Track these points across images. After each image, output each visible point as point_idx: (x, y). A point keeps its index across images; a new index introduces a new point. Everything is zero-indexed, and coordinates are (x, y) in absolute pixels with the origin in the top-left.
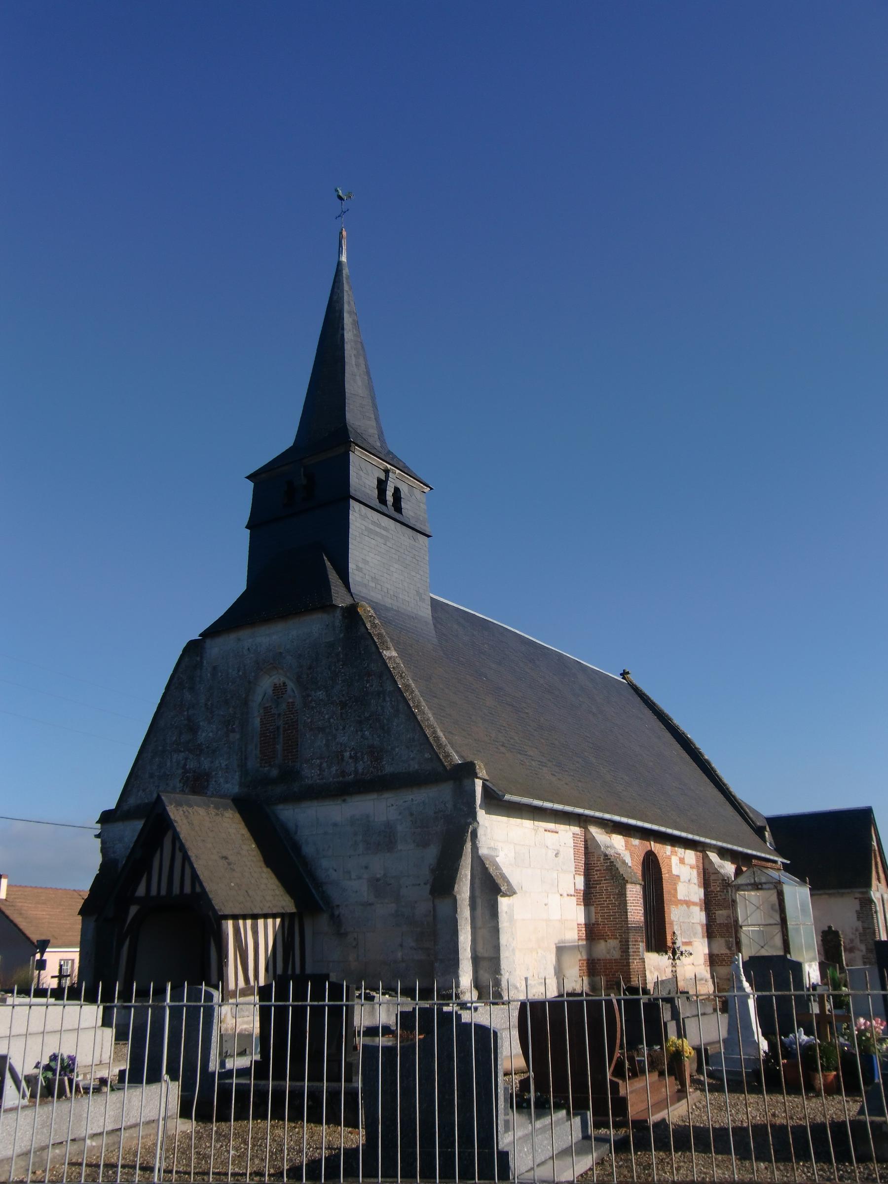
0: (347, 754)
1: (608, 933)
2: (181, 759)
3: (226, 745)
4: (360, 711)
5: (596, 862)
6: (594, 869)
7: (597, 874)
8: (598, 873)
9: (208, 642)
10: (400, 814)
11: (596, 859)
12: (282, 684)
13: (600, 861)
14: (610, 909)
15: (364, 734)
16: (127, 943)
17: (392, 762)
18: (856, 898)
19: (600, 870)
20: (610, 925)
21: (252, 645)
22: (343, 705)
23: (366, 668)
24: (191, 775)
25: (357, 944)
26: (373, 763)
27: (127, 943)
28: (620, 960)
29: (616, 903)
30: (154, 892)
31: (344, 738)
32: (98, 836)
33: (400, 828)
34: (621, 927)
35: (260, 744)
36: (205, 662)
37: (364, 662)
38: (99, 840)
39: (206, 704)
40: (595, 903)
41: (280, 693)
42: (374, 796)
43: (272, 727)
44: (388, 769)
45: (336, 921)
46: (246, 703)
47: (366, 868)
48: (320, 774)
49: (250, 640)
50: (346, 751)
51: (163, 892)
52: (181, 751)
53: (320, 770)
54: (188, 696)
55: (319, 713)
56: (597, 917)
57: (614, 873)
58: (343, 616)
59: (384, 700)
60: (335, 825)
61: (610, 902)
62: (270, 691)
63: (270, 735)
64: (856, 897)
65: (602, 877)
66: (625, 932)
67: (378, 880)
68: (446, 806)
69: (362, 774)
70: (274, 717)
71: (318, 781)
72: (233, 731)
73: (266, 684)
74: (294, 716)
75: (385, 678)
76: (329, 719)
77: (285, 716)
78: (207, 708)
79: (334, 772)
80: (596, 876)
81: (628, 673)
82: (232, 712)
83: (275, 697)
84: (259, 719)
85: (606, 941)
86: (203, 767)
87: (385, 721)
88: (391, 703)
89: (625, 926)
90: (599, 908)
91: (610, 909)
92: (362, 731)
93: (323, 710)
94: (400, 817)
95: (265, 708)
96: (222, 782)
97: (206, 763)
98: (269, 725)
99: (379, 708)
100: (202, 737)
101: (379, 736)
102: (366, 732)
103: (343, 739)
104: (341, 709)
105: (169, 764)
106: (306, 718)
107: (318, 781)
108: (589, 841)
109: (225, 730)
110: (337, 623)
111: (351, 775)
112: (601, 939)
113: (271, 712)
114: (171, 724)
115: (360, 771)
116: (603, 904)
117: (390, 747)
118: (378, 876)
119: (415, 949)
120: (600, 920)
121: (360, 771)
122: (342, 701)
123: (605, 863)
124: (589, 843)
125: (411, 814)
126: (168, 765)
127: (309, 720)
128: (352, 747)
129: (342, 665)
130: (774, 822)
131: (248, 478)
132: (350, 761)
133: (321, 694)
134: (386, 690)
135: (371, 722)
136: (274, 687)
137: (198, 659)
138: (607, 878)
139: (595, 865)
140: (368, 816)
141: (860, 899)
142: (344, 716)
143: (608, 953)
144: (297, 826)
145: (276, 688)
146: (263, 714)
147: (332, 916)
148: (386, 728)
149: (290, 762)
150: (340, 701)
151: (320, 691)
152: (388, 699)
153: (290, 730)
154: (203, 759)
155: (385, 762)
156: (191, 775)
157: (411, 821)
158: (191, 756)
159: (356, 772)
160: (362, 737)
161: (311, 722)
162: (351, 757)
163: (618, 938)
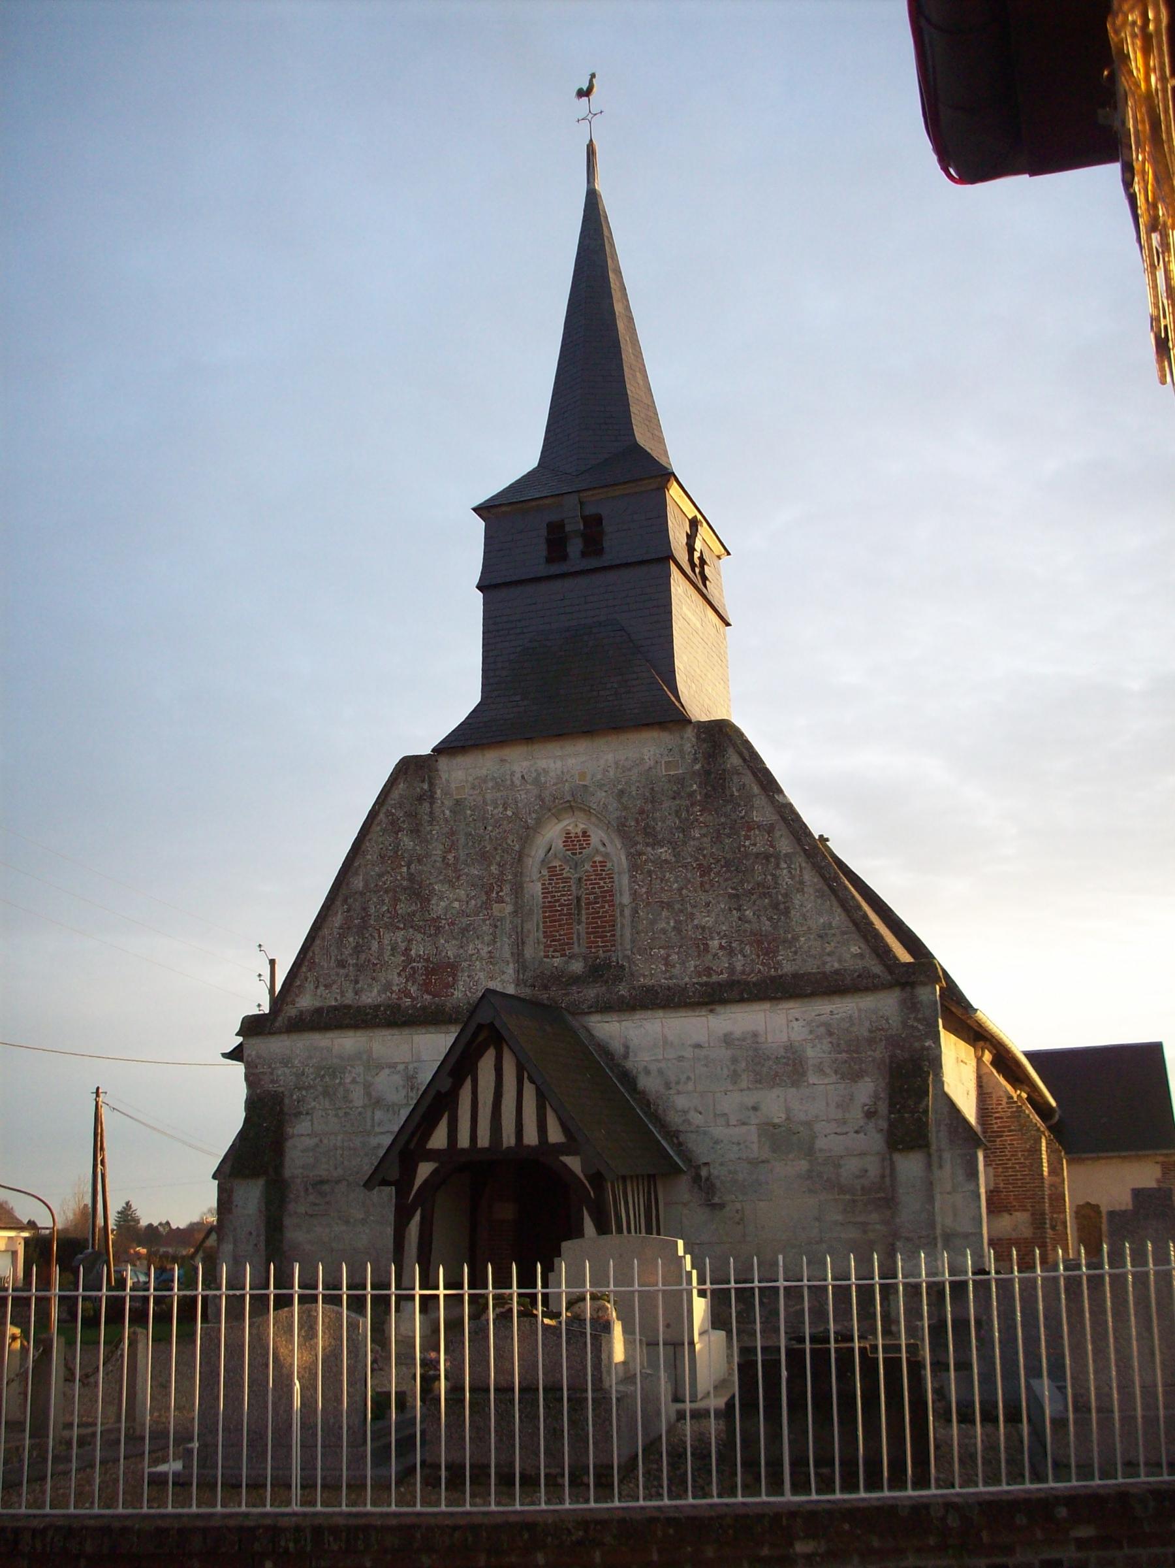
0: (714, 944)
1: (1015, 1204)
2: (399, 940)
3: (488, 922)
4: (735, 881)
5: (994, 1106)
6: (991, 1116)
7: (996, 1123)
8: (998, 1121)
9: (443, 763)
10: (811, 1032)
11: (994, 1102)
12: (581, 834)
13: (1001, 1104)
14: (1018, 1171)
15: (744, 915)
16: (417, 1218)
17: (795, 957)
18: (1157, 1163)
19: (1002, 1118)
20: (1016, 1193)
21: (529, 771)
22: (705, 871)
23: (743, 818)
24: (420, 965)
25: (742, 1219)
26: (762, 957)
27: (417, 1218)
28: (1032, 1238)
29: (1027, 1162)
30: (464, 1141)
31: (707, 919)
32: (235, 1054)
33: (810, 1053)
34: (1033, 1195)
35: (545, 922)
36: (439, 792)
37: (740, 809)
38: (239, 1068)
39: (444, 858)
40: (994, 1163)
41: (577, 847)
42: (766, 1006)
43: (565, 898)
44: (788, 968)
45: (705, 1187)
46: (520, 857)
47: (755, 1108)
48: (667, 971)
49: (525, 764)
50: (712, 939)
51: (484, 1141)
52: (398, 928)
53: (666, 965)
54: (407, 842)
55: (662, 880)
56: (997, 1181)
57: (1023, 1121)
58: (698, 737)
59: (777, 866)
60: (698, 1046)
61: (1017, 1161)
62: (559, 844)
63: (563, 910)
64: (1157, 1160)
65: (1005, 1127)
66: (1039, 1202)
67: (775, 1126)
68: (889, 1023)
69: (743, 972)
70: (570, 882)
71: (663, 981)
72: (500, 900)
73: (553, 833)
74: (605, 883)
75: (778, 834)
76: (680, 889)
77: (588, 882)
78: (447, 864)
79: (692, 969)
80: (995, 1126)
81: (827, 840)
82: (497, 872)
83: (569, 853)
84: (539, 885)
85: (1011, 1214)
86: (443, 954)
87: (780, 897)
88: (790, 872)
89: (1040, 1193)
90: (1000, 1170)
91: (1018, 1171)
92: (740, 910)
93: (668, 875)
94: (810, 1037)
95: (549, 868)
96: (481, 977)
97: (450, 950)
98: (559, 894)
99: (769, 877)
100: (438, 907)
101: (770, 919)
102: (747, 912)
103: (709, 921)
104: (701, 876)
105: (375, 945)
106: (637, 887)
107: (663, 981)
108: (984, 1077)
109: (484, 898)
110: (688, 747)
111: (722, 973)
112: (1003, 1211)
113: (562, 874)
114: (376, 885)
115: (739, 968)
116: (1006, 1164)
117: (790, 936)
118: (776, 1121)
119: (842, 1224)
120: (1002, 1185)
121: (739, 968)
122: (702, 864)
123: (1009, 1108)
124: (985, 1080)
125: (830, 1034)
126: (373, 949)
127: (644, 890)
128: (722, 934)
129: (700, 811)
130: (1038, 1058)
131: (475, 509)
132: (721, 953)
133: (664, 852)
134: (780, 852)
135: (754, 897)
136: (566, 837)
137: (426, 786)
138: (1013, 1128)
139: (993, 1111)
140: (755, 1035)
141: (1163, 1164)
142: (707, 886)
143: (1014, 1230)
144: (627, 1047)
145: (568, 838)
146: (547, 878)
147: (697, 1178)
148: (782, 906)
149: (601, 952)
150: (697, 865)
151: (662, 847)
152: (784, 865)
153: (598, 903)
154: (442, 941)
155: (781, 957)
156: (420, 965)
157: (831, 1042)
158: (419, 936)
159: (732, 970)
160: (740, 919)
161: (646, 893)
162: (721, 947)
163: (1029, 1210)
